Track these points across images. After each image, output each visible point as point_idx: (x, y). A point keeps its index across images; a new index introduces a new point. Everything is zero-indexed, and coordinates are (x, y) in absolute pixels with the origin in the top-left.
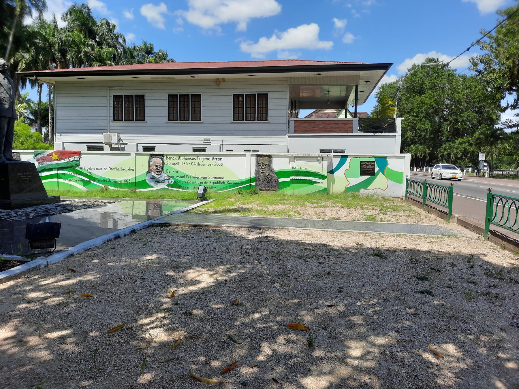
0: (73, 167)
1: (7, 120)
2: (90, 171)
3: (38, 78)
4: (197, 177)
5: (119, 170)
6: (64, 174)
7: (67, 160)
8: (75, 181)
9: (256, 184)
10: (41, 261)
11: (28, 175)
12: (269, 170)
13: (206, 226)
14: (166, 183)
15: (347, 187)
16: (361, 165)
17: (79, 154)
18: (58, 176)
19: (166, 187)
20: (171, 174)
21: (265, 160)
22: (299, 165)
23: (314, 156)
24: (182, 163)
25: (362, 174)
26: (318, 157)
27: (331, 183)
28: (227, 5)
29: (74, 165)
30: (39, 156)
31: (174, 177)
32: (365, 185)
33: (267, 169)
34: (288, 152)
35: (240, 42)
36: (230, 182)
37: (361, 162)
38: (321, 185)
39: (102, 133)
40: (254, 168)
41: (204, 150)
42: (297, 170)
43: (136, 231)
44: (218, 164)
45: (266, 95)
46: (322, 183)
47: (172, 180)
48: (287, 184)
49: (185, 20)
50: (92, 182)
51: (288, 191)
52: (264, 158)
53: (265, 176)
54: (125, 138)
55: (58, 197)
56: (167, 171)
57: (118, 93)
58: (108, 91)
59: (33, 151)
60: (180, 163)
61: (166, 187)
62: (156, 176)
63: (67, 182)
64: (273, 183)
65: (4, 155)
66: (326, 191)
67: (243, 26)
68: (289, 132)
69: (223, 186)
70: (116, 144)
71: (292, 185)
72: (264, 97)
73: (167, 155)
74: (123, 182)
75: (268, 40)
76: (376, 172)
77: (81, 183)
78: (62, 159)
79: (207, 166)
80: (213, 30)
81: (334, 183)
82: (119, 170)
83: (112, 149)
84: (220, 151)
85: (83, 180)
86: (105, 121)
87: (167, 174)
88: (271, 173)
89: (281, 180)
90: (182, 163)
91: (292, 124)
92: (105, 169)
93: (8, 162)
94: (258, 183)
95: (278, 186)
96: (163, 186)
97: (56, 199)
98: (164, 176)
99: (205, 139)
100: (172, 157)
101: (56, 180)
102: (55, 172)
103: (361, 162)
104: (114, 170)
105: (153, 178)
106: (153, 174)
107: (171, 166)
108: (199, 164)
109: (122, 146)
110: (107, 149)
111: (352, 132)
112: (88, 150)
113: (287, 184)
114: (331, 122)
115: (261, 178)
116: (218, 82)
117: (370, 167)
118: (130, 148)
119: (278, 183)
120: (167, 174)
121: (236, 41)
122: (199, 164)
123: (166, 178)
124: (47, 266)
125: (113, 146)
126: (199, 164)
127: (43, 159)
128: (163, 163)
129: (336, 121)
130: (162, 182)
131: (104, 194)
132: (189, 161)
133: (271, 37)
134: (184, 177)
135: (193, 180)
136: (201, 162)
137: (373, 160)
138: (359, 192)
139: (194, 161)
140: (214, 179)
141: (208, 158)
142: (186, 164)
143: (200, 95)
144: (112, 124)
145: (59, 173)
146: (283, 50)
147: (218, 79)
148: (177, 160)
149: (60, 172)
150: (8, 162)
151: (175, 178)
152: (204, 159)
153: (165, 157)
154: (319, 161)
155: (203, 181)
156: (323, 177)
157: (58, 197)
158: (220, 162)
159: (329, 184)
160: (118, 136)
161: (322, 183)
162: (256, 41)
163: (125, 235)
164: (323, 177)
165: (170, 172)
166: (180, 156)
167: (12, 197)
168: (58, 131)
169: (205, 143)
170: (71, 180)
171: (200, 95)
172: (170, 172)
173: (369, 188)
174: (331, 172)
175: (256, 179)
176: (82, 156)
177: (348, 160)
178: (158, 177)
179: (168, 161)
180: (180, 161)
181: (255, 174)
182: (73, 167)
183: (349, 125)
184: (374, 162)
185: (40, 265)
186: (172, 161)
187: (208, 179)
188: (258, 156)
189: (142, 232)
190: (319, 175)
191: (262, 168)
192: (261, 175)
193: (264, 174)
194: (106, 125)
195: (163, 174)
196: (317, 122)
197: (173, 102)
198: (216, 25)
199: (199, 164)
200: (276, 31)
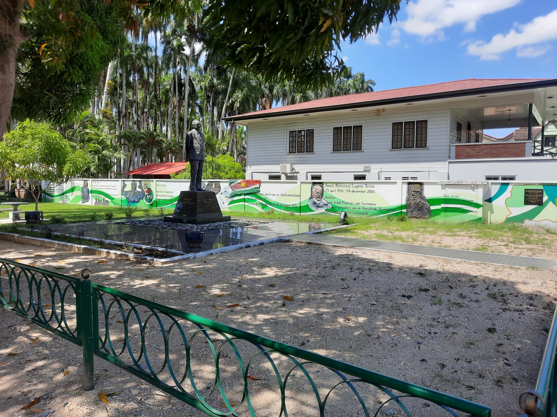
0: (254, 193)
1: (198, 162)
2: (267, 196)
3: (235, 122)
4: (351, 203)
5: (288, 195)
6: (249, 199)
7: (251, 188)
8: (257, 204)
9: (407, 211)
10: (191, 255)
11: (210, 200)
12: (421, 197)
13: (324, 245)
14: (325, 208)
15: (508, 217)
16: (526, 193)
17: (259, 182)
18: (244, 200)
19: (325, 211)
20: (329, 200)
21: (416, 188)
22: (452, 193)
23: (467, 183)
24: (339, 190)
25: (527, 202)
26: (471, 185)
27: (489, 212)
28: (452, 6)
29: (255, 191)
30: (232, 184)
31: (331, 203)
32: (531, 215)
33: (418, 196)
34: (449, 179)
35: (467, 45)
36: (382, 209)
37: (525, 190)
38: (475, 214)
39: (279, 164)
40: (405, 195)
41: (363, 178)
42: (448, 198)
43: (265, 244)
44: (370, 192)
45: (426, 122)
46: (477, 212)
47: (330, 206)
48: (438, 212)
49: (402, 31)
50: (268, 205)
51: (440, 219)
52: (416, 186)
53: (416, 204)
54: (297, 168)
55: (230, 217)
56: (326, 197)
57: (293, 129)
58: (286, 128)
59: (229, 180)
60: (337, 190)
61: (325, 211)
62: (317, 201)
63: (250, 205)
64: (425, 210)
65: (196, 186)
66: (482, 221)
67: (471, 26)
68: (449, 157)
69: (375, 212)
70: (290, 173)
71: (443, 213)
72: (423, 124)
73: (327, 183)
74: (291, 206)
75: (505, 36)
76: (544, 201)
77: (261, 206)
78: (247, 187)
79: (360, 193)
80: (434, 37)
81: (492, 212)
82: (288, 195)
83: (288, 177)
84: (379, 179)
85: (262, 204)
86: (283, 154)
87: (326, 199)
88: (422, 201)
89: (432, 208)
90: (339, 190)
91: (453, 149)
92: (278, 195)
93: (197, 192)
94: (409, 210)
95: (430, 213)
96: (322, 210)
97: (228, 219)
98: (324, 201)
99: (365, 167)
100: (348, 185)
101: (243, 203)
102: (242, 197)
103: (525, 190)
104: (284, 196)
105: (315, 203)
106: (315, 200)
107: (330, 192)
108: (354, 191)
109: (295, 175)
110: (283, 177)
111: (524, 156)
112: (269, 179)
113: (438, 212)
114: (500, 146)
115: (412, 205)
116: (378, 113)
117: (537, 196)
118: (301, 177)
119: (429, 211)
120: (326, 199)
121: (462, 44)
122: (353, 191)
123: (325, 203)
124: (194, 258)
125: (288, 175)
126: (353, 191)
127: (235, 187)
128: (323, 190)
129: (505, 145)
130: (321, 207)
131: (269, 216)
132: (345, 189)
133: (508, 32)
134: (340, 203)
135: (347, 206)
136: (355, 189)
137: (541, 187)
138: (523, 222)
139: (349, 189)
140: (366, 205)
141: (362, 185)
142: (342, 191)
143: (362, 126)
144: (288, 157)
145: (39, 210)
146: (525, 47)
147: (379, 110)
148: (335, 188)
149: (247, 197)
150: (197, 192)
151: (333, 203)
152: (358, 186)
153: (325, 185)
154: (473, 189)
155: (357, 207)
156: (477, 206)
157: (230, 217)
158: (372, 189)
159: (485, 214)
160: (291, 165)
161: (477, 212)
162: (488, 40)
163: (255, 246)
164: (477, 206)
165: (328, 198)
166: (337, 183)
167: (198, 215)
168: (249, 163)
169: (365, 171)
170: (254, 204)
171: (362, 126)
172: (328, 198)
173: (535, 219)
174: (490, 200)
175: (407, 206)
176: (262, 184)
177: (510, 187)
178: (318, 202)
179: (327, 188)
180: (337, 188)
181: (406, 201)
182: (254, 193)
183: (521, 148)
184: (542, 190)
185: (190, 257)
186: (330, 189)
187: (361, 205)
188: (409, 183)
189: (268, 245)
190: (473, 204)
191: (413, 195)
192: (413, 203)
193: (415, 201)
194: (283, 157)
195: (322, 200)
196: (482, 146)
197: (338, 134)
198: (437, 30)
199: (354, 191)
200: (515, 24)
